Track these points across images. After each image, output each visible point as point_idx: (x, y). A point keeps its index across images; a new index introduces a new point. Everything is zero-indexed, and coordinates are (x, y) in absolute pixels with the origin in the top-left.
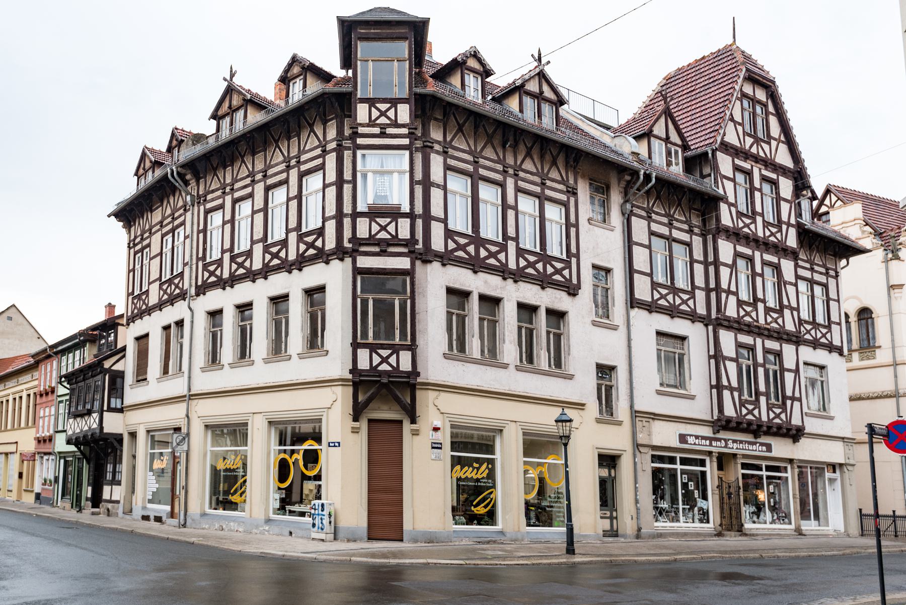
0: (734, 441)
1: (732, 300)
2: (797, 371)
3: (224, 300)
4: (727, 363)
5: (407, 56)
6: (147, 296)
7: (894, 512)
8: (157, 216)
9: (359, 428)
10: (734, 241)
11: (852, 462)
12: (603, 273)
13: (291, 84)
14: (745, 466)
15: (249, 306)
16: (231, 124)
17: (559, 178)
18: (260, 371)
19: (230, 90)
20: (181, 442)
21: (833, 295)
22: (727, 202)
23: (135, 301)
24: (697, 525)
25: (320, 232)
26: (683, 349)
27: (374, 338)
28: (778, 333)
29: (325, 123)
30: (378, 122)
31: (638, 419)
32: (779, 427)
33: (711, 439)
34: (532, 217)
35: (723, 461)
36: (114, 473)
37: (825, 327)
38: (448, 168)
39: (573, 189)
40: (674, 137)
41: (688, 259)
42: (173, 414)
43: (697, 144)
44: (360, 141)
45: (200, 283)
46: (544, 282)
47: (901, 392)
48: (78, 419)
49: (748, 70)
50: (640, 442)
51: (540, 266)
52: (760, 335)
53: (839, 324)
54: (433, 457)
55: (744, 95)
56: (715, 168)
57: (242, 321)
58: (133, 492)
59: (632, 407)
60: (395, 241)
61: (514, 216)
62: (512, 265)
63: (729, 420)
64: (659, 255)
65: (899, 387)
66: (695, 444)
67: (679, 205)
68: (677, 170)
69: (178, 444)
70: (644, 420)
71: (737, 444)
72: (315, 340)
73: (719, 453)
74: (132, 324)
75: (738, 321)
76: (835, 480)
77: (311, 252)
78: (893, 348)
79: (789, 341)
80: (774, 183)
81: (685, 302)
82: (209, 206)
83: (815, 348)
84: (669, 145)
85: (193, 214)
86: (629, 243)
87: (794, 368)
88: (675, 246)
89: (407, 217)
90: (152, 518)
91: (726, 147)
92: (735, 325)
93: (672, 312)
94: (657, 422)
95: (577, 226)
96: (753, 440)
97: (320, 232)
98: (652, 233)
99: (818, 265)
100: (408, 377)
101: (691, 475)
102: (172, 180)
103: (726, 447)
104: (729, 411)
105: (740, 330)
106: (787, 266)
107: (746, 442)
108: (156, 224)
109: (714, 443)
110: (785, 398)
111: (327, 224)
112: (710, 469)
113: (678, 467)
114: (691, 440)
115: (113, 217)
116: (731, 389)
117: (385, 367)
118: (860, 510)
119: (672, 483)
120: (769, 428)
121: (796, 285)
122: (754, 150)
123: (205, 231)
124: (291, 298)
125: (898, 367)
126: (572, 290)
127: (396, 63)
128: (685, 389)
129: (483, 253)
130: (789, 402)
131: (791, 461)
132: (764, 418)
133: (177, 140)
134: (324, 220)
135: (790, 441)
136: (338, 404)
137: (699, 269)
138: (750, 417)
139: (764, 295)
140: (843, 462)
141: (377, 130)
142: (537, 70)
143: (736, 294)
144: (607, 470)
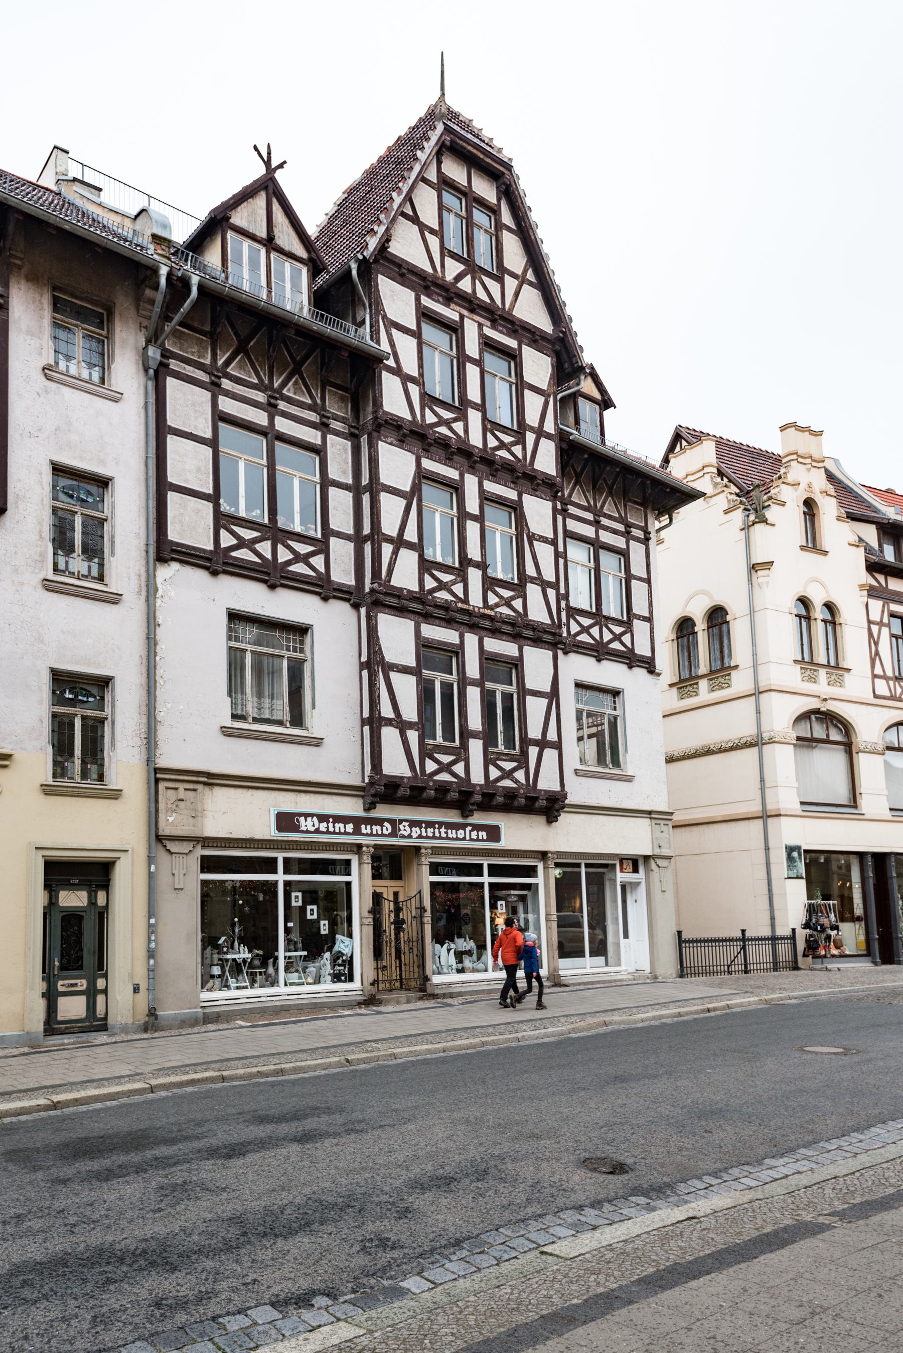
0: (413, 824)
2: (554, 694)
4: (394, 676)
7: (743, 931)
10: (418, 448)
11: (665, 852)
14: (435, 869)
21: (638, 569)
22: (397, 371)
24: (328, 986)
26: (302, 651)
28: (513, 625)
32: (511, 795)
33: (357, 822)
35: (391, 863)
37: (619, 622)
41: (623, 574)
47: (766, 736)
49: (448, 130)
50: (165, 829)
52: (473, 627)
55: (445, 184)
56: (377, 305)
64: (611, 578)
65: (764, 728)
66: (317, 831)
67: (297, 370)
70: (662, 822)
71: (409, 825)
73: (376, 846)
76: (638, 884)
78: (755, 666)
79: (537, 642)
81: (617, 638)
83: (630, 667)
86: (161, 430)
87: (547, 688)
88: (604, 556)
91: (405, 273)
92: (414, 606)
93: (272, 576)
94: (218, 791)
96: (460, 820)
99: (610, 517)
101: (311, 894)
103: (394, 834)
104: (395, 764)
105: (427, 617)
106: (538, 512)
107: (441, 824)
109: (365, 829)
110: (526, 742)
112: (360, 882)
113: (280, 877)
114: (307, 824)
116: (402, 726)
118: (679, 933)
119: (251, 912)
122: (465, 285)
130: (533, 751)
131: (543, 855)
132: (477, 778)
135: (542, 819)
138: (444, 777)
139: (483, 554)
140: (649, 852)
143: (418, 547)
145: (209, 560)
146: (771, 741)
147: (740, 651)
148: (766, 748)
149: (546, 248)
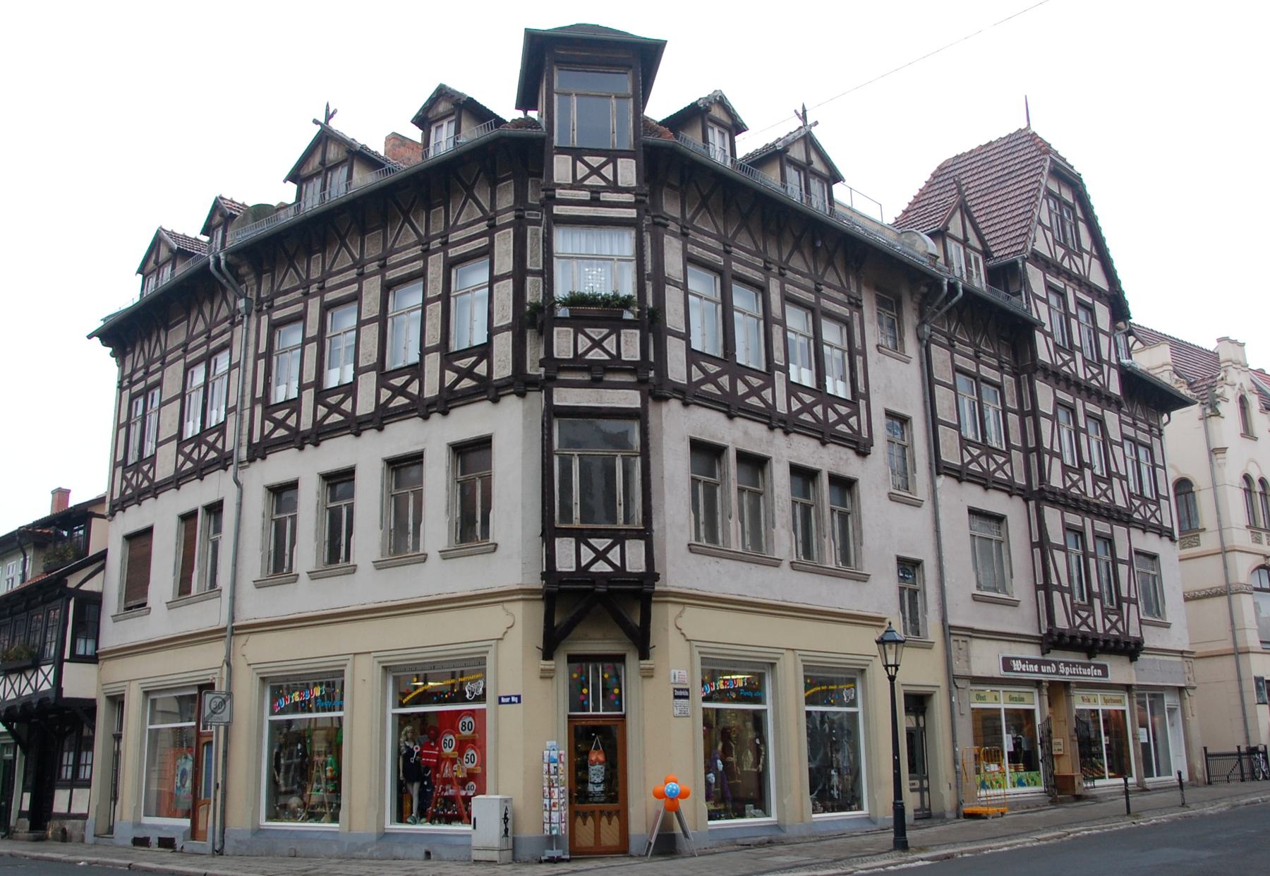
1: (1056, 464)
3: (304, 467)
4: (1055, 552)
5: (630, 91)
6: (153, 465)
8: (177, 336)
9: (553, 670)
12: (898, 424)
13: (433, 129)
15: (347, 475)
16: (324, 187)
17: (838, 284)
18: (367, 584)
19: (325, 137)
20: (218, 707)
23: (129, 475)
25: (484, 352)
27: (582, 521)
28: (1108, 510)
29: (494, 183)
30: (586, 183)
31: (953, 638)
34: (800, 343)
36: (77, 766)
38: (689, 260)
39: (857, 299)
40: (974, 241)
42: (201, 662)
43: (1002, 252)
44: (557, 210)
45: (256, 440)
46: (824, 435)
47: (1233, 588)
48: (13, 677)
49: (1052, 161)
51: (818, 410)
52: (1088, 512)
53: (1167, 498)
54: (677, 712)
56: (1025, 282)
57: (278, 512)
58: (115, 798)
59: (944, 620)
60: (616, 364)
61: (780, 336)
62: (782, 408)
63: (1061, 634)
68: (980, 283)
69: (213, 712)
72: (471, 525)
74: (119, 514)
75: (1064, 494)
77: (467, 383)
78: (1220, 530)
79: (1120, 521)
80: (1090, 309)
82: (277, 315)
84: (968, 250)
85: (248, 329)
86: (929, 383)
89: (635, 328)
90: (154, 841)
91: (1036, 258)
93: (985, 482)
95: (863, 353)
96: (1087, 661)
97: (484, 352)
98: (957, 370)
100: (641, 583)
102: (216, 274)
103: (1057, 673)
104: (1061, 622)
106: (1111, 418)
108: (177, 348)
111: (497, 339)
114: (1017, 665)
115: (96, 340)
117: (601, 567)
118: (1205, 749)
120: (1106, 642)
121: (1122, 445)
122: (1066, 264)
123: (268, 355)
124: (496, 444)
125: (1229, 555)
126: (862, 449)
127: (614, 101)
128: (1005, 592)
129: (742, 389)
130: (1125, 605)
133: (222, 216)
134: (492, 331)
135: (1126, 659)
136: (518, 631)
137: (1013, 419)
141: (585, 195)
142: (803, 132)
144: (913, 718)
145: (959, 472)
146: (1238, 592)
147: (1206, 515)
148: (1234, 597)
149: (1105, 233)
